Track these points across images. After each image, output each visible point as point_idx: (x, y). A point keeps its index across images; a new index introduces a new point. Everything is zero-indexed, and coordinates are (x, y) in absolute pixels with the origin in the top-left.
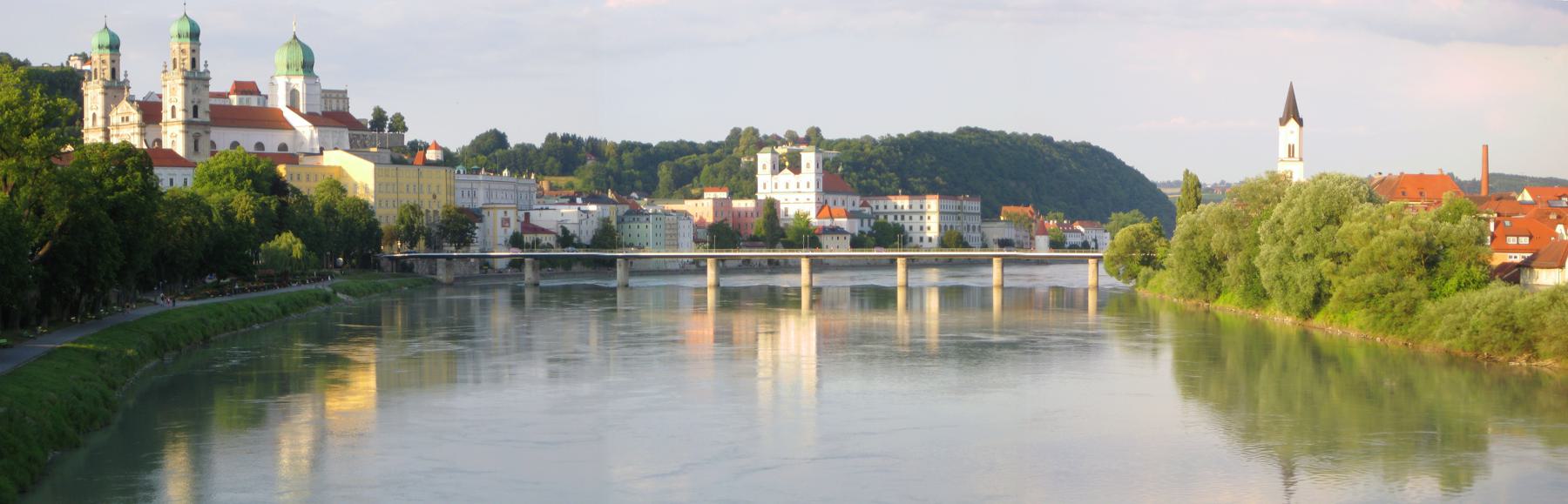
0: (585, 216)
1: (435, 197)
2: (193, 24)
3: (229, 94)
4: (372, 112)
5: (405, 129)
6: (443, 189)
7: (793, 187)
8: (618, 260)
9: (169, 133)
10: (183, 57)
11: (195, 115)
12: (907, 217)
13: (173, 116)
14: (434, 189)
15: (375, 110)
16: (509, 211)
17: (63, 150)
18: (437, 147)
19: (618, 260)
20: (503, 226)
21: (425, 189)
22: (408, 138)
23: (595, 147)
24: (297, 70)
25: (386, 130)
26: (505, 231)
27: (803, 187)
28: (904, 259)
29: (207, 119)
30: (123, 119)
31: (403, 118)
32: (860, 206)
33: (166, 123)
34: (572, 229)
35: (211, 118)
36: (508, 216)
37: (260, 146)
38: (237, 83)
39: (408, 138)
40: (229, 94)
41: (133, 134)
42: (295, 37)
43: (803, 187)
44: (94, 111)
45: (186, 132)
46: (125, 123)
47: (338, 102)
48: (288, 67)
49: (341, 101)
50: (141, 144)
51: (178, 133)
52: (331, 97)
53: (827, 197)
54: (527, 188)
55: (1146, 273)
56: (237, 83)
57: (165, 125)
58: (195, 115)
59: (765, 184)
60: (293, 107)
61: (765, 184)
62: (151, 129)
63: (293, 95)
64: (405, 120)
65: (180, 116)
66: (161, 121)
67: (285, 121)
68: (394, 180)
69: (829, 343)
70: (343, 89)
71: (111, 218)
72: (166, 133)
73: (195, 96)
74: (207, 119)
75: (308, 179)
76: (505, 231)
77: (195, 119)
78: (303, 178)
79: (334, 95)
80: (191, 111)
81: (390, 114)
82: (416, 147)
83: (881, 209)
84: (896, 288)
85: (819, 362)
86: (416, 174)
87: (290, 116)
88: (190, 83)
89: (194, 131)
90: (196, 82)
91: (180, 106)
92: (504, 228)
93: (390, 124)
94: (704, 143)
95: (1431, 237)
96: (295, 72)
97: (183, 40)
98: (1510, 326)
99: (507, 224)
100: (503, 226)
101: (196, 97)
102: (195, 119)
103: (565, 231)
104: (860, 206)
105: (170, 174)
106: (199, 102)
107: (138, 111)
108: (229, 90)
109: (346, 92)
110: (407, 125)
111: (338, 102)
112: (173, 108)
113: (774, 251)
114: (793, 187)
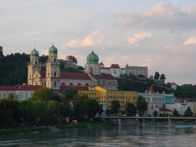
1: (128, 100)
2: (55, 48)
5: (165, 78)
11: (55, 75)
13: (49, 76)
20: (151, 109)
21: (125, 98)
22: (166, 82)
24: (93, 62)
26: (152, 110)
29: (59, 76)
30: (37, 77)
33: (47, 78)
34: (178, 110)
35: (60, 76)
37: (71, 84)
39: (166, 82)
47: (144, 70)
48: (90, 61)
49: (145, 70)
50: (40, 84)
51: (49, 80)
52: (142, 69)
57: (47, 78)
58: (55, 75)
62: (43, 79)
66: (45, 77)
70: (145, 66)
71: (163, 122)
72: (47, 80)
73: (55, 70)
74: (59, 76)
75: (130, 94)
76: (152, 110)
78: (91, 94)
80: (54, 74)
81: (160, 74)
88: (53, 66)
89: (54, 80)
90: (56, 65)
96: (92, 63)
97: (52, 53)
100: (151, 109)
101: (55, 70)
103: (175, 110)
106: (56, 71)
107: (40, 74)
109: (147, 67)
111: (144, 70)
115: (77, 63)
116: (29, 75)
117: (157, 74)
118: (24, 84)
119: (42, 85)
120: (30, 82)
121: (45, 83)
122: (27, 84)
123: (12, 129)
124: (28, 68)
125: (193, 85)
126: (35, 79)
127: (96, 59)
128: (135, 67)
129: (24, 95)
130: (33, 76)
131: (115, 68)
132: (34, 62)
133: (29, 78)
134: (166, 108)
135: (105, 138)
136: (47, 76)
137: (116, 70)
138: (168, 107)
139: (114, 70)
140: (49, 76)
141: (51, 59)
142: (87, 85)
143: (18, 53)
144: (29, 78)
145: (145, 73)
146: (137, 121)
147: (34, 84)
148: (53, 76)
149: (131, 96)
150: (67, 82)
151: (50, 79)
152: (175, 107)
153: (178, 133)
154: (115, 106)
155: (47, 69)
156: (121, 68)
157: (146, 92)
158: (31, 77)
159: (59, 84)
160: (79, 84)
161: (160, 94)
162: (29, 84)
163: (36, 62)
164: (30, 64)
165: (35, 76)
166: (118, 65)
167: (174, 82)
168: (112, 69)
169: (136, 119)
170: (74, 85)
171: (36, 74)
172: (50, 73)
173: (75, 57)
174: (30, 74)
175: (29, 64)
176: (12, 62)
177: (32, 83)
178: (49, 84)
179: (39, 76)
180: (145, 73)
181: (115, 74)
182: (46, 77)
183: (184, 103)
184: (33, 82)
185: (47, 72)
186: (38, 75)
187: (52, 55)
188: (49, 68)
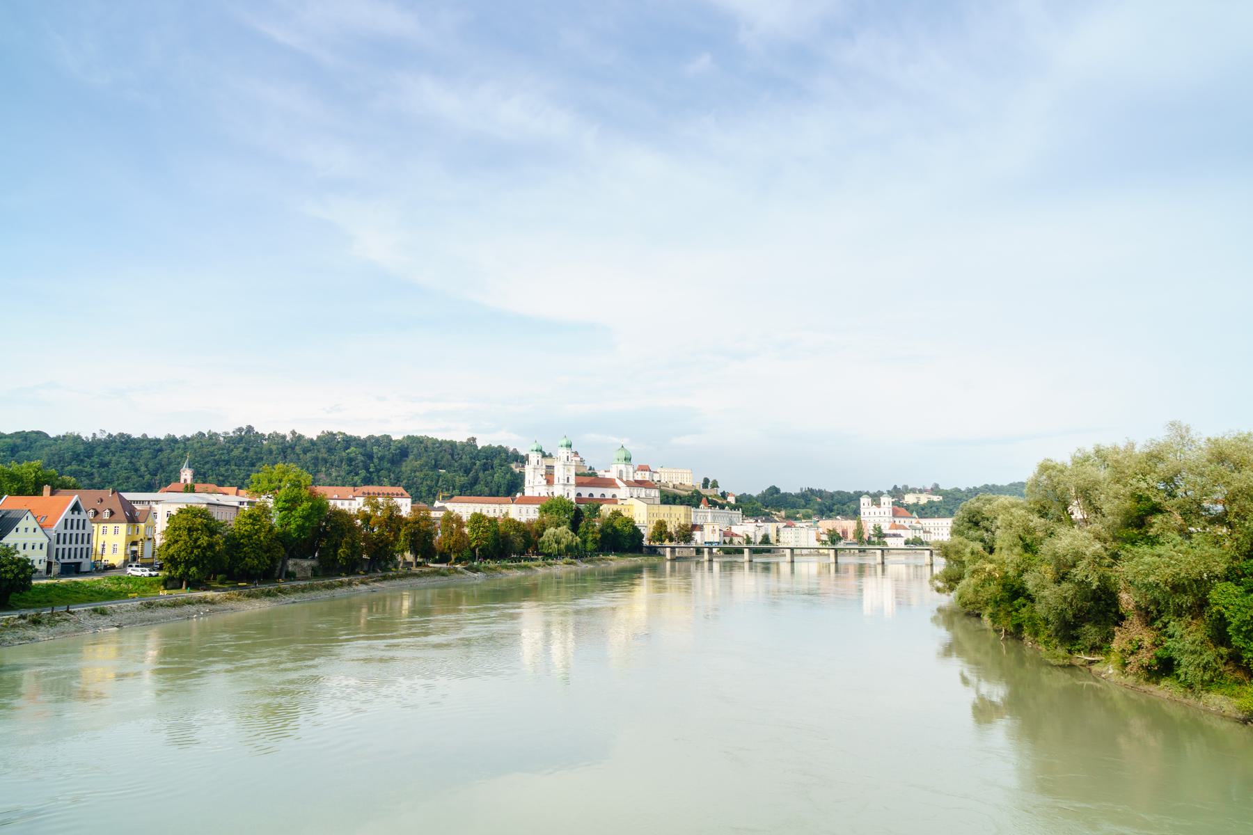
1: (678, 519)
6: (683, 515)
7: (877, 514)
11: (568, 481)
12: (940, 529)
14: (678, 516)
17: (941, 498)
23: (820, 493)
27: (882, 514)
32: (890, 529)
37: (591, 495)
42: (622, 447)
43: (882, 514)
53: (895, 519)
54: (737, 516)
58: (568, 481)
59: (41, 548)
60: (621, 479)
61: (41, 548)
67: (616, 484)
68: (657, 512)
69: (1121, 473)
82: (724, 495)
83: (927, 525)
86: (669, 508)
87: (618, 482)
95: (1056, 480)
98: (1139, 495)
104: (890, 529)
114: (877, 514)
117: (706, 481)
120: (528, 492)
122: (523, 493)
125: (362, 438)
129: (491, 511)
138: (735, 530)
139: (642, 474)
142: (614, 496)
146: (692, 551)
148: (566, 482)
149: (676, 516)
150: (585, 492)
152: (745, 529)
153: (217, 611)
154: (661, 528)
160: (603, 495)
161: (722, 511)
162: (526, 495)
166: (648, 466)
169: (692, 549)
170: (583, 496)
183: (758, 524)
188: (559, 471)
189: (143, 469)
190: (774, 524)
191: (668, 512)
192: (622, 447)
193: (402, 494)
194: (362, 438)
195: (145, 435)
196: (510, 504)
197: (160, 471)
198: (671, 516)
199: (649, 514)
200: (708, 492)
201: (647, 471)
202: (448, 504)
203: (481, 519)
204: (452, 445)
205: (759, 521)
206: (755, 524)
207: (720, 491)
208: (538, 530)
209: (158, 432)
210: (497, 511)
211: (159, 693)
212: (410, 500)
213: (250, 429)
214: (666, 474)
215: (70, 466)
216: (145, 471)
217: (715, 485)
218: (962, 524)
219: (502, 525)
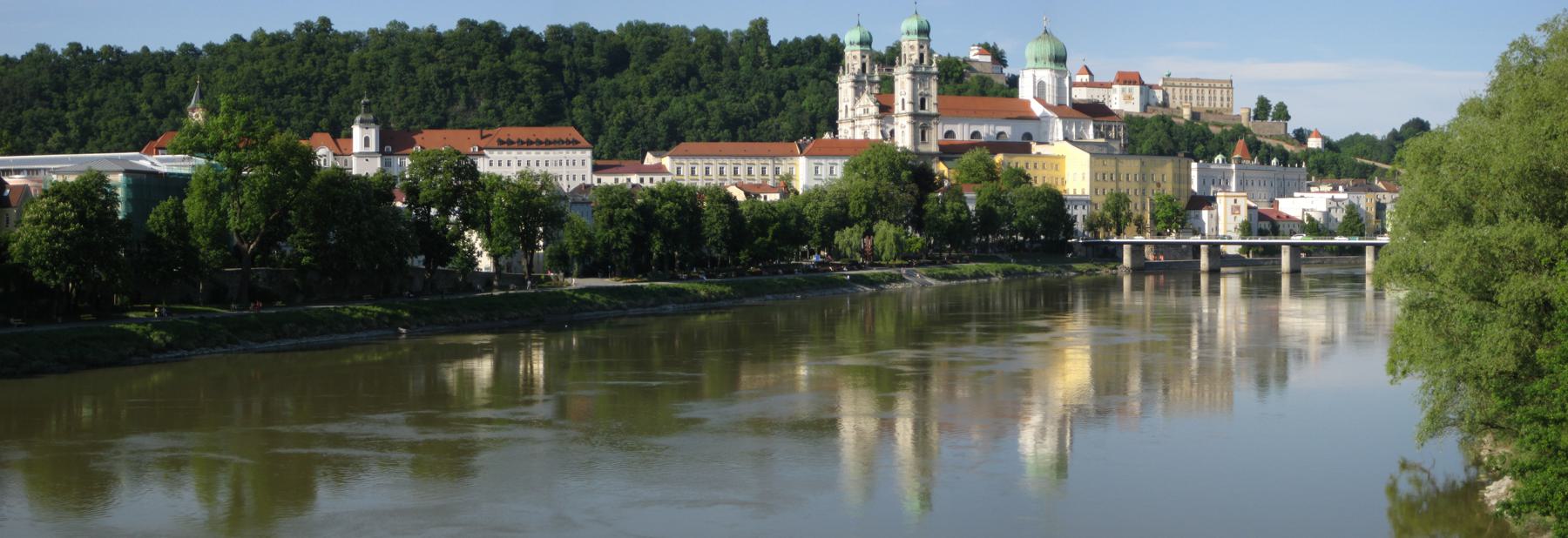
0: (1334, 204)
3: (1112, 84)
4: (1257, 101)
8: (1283, 246)
9: (899, 124)
10: (912, 53)
13: (903, 108)
15: (1259, 99)
16: (1238, 199)
18: (1318, 135)
19: (1283, 246)
20: (1233, 213)
25: (1270, 119)
28: (1240, 247)
31: (1286, 107)
36: (1238, 203)
38: (1120, 74)
40: (1112, 84)
41: (871, 125)
42: (1046, 32)
44: (903, 96)
45: (914, 125)
46: (866, 115)
48: (1036, 60)
55: (1391, 262)
56: (1120, 74)
58: (923, 107)
60: (1041, 100)
63: (1040, 88)
64: (1288, 109)
65: (909, 108)
76: (1235, 218)
77: (922, 112)
79: (1218, 85)
81: (1274, 103)
82: (1301, 136)
84: (1364, 275)
85: (1200, 353)
91: (908, 98)
92: (1234, 216)
93: (1273, 113)
94: (1334, 141)
97: (911, 37)
99: (1237, 212)
100: (1233, 213)
102: (922, 112)
105: (790, 164)
108: (1112, 80)
110: (1290, 113)
111: (1222, 91)
112: (903, 100)
113: (1276, 239)
115: (1005, 66)
116: (841, 107)
117: (1263, 105)
118: (827, 136)
119: (880, 137)
120: (845, 131)
121: (892, 132)
123: (446, 298)
124: (840, 86)
126: (860, 118)
127: (1060, 54)
128: (1192, 80)
130: (853, 110)
131: (1130, 83)
132: (858, 66)
133: (841, 115)
134: (1280, 210)
135: (628, 373)
136: (898, 109)
137: (1130, 91)
139: (1123, 90)
140: (903, 108)
141: (911, 55)
143: (814, 34)
144: (844, 116)
145: (1225, 99)
147: (859, 136)
151: (908, 119)
155: (897, 86)
156: (1146, 83)
157: (1218, 161)
158: (850, 114)
159: (936, 135)
160: (975, 135)
163: (864, 65)
164: (844, 74)
165: (859, 112)
167: (261, 28)
168: (1117, 87)
171: (862, 103)
172: (907, 101)
173: (1000, 47)
174: (844, 105)
175: (841, 71)
176: (797, 67)
177: (850, 131)
178: (903, 137)
179: (874, 110)
180: (1225, 99)
181: (1126, 103)
182: (896, 112)
184: (854, 128)
185: (898, 98)
186: (868, 103)
187: (911, 43)
189: (144, 107)
190: (1371, 195)
191: (1113, 170)
192: (1046, 32)
193: (577, 142)
194: (1379, 138)
195: (146, 49)
196: (797, 156)
197: (172, 112)
198: (1118, 180)
199: (1094, 177)
200: (1265, 131)
201: (1135, 83)
202: (653, 163)
203: (73, 189)
204: (716, 38)
205: (1341, 188)
206: (1330, 196)
207: (1292, 126)
208: (563, 216)
209: (164, 39)
210: (769, 171)
211: (1189, 310)
212: (589, 153)
213: (325, 22)
214: (1177, 89)
215: (30, 110)
216: (148, 112)
217: (1283, 114)
218: (1540, 206)
219: (199, 219)
